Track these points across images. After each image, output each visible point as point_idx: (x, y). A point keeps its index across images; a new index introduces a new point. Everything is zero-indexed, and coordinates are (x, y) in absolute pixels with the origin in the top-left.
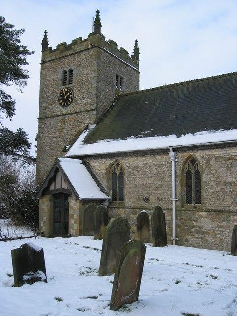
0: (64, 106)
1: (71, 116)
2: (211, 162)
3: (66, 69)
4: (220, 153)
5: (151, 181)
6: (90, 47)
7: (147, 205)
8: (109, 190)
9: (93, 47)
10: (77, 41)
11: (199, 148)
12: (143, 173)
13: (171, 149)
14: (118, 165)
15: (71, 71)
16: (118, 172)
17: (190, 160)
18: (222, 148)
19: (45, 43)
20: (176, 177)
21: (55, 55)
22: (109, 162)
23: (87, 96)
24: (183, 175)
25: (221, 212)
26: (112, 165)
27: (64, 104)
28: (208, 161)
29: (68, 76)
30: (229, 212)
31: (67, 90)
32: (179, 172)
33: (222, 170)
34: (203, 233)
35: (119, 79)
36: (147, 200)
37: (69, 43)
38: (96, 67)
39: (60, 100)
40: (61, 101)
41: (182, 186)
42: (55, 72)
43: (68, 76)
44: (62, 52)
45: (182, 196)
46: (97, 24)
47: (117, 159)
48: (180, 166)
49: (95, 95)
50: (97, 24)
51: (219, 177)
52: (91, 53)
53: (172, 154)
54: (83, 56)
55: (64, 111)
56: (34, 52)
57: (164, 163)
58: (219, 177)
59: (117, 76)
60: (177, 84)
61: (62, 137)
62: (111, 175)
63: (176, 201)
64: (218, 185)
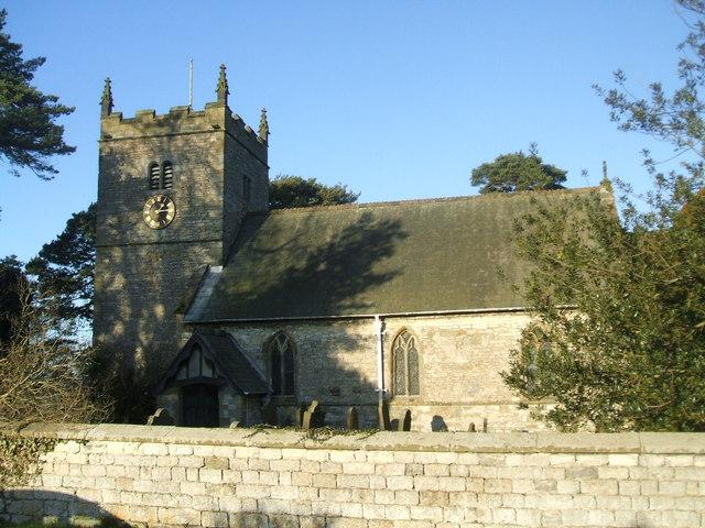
2: (435, 338)
6: (209, 127)
14: (282, 338)
16: (282, 349)
25: (450, 404)
28: (431, 335)
30: (460, 404)
33: (450, 350)
46: (224, 91)
51: (446, 358)
58: (446, 358)
59: (245, 177)
64: (444, 367)
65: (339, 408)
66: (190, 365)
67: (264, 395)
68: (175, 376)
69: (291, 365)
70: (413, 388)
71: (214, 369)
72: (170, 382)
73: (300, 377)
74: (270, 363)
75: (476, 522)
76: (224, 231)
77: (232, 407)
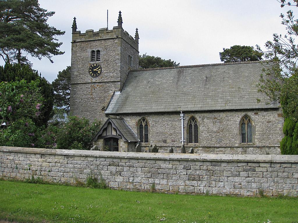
0: (93, 77)
1: (100, 84)
3: (95, 50)
4: (210, 115)
5: (167, 130)
7: (165, 145)
8: (138, 135)
9: (117, 37)
10: (105, 31)
11: (197, 112)
12: (162, 125)
13: (181, 112)
14: (144, 120)
15: (98, 51)
17: (192, 118)
18: (210, 112)
19: (74, 27)
20: (184, 128)
21: (85, 38)
22: (138, 118)
23: (113, 71)
24: (187, 127)
26: (140, 120)
27: (94, 75)
29: (95, 55)
31: (96, 65)
32: (186, 125)
33: (211, 125)
34: (294, 127)
35: (130, 57)
36: (165, 141)
37: (96, 30)
38: (120, 52)
39: (90, 71)
40: (91, 73)
41: (187, 133)
42: (83, 50)
43: (95, 55)
44: (90, 37)
45: (187, 139)
46: (120, 21)
47: (144, 116)
48: (186, 122)
49: (119, 71)
50: (120, 21)
52: (116, 41)
53: (182, 115)
54: (109, 43)
55: (94, 80)
56: (65, 32)
57: (176, 120)
59: (129, 56)
60: (159, 59)
61: (92, 98)
62: (139, 126)
63: (184, 142)
65: (166, 148)
66: (107, 131)
67: (137, 142)
68: (101, 134)
69: (147, 130)
70: (147, 141)
71: (116, 132)
72: (100, 137)
73: (151, 135)
74: (139, 130)
75: (210, 187)
76: (121, 77)
77: (124, 147)
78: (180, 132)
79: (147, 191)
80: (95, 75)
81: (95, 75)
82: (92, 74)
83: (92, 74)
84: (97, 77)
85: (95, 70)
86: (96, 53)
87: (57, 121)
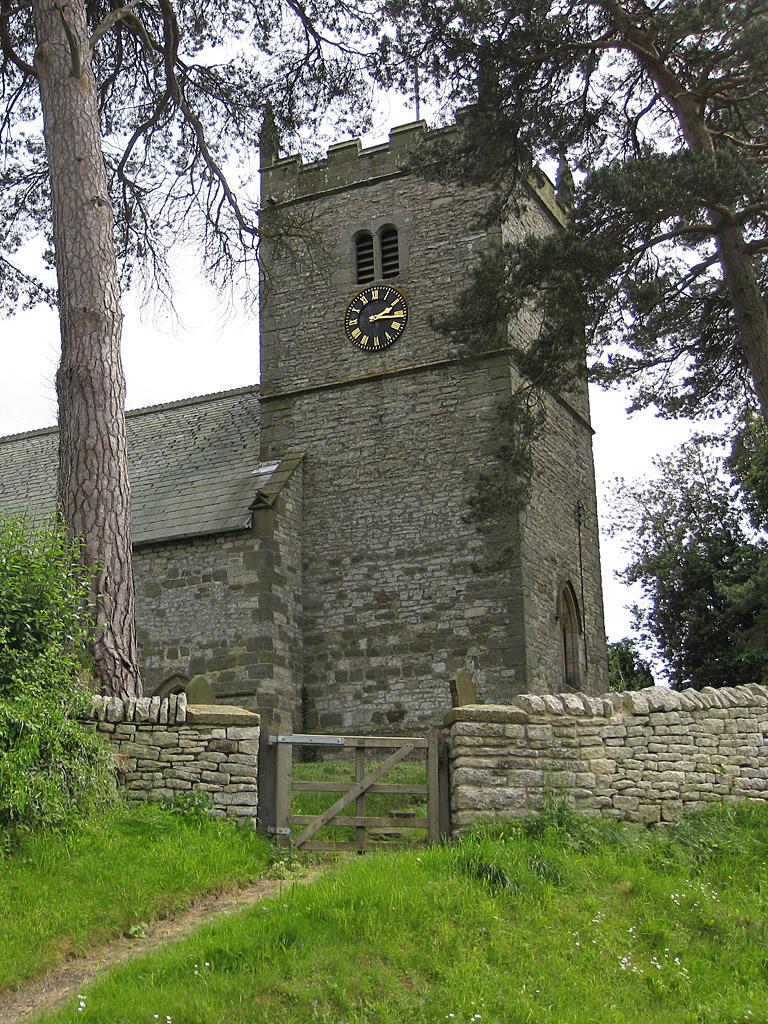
15: (389, 233)
27: (383, 340)
78: (134, 559)
79: (450, 808)
80: (376, 342)
81: (376, 342)
82: (360, 337)
83: (360, 337)
84: (384, 349)
85: (379, 316)
86: (376, 242)
87: (398, 705)
